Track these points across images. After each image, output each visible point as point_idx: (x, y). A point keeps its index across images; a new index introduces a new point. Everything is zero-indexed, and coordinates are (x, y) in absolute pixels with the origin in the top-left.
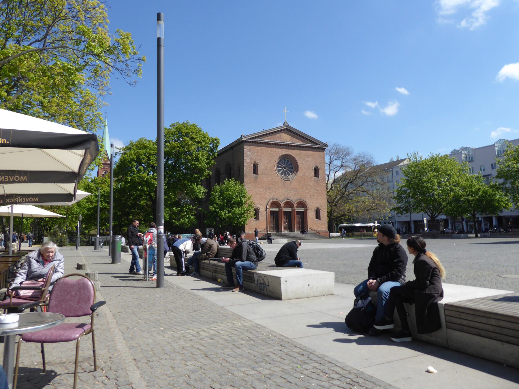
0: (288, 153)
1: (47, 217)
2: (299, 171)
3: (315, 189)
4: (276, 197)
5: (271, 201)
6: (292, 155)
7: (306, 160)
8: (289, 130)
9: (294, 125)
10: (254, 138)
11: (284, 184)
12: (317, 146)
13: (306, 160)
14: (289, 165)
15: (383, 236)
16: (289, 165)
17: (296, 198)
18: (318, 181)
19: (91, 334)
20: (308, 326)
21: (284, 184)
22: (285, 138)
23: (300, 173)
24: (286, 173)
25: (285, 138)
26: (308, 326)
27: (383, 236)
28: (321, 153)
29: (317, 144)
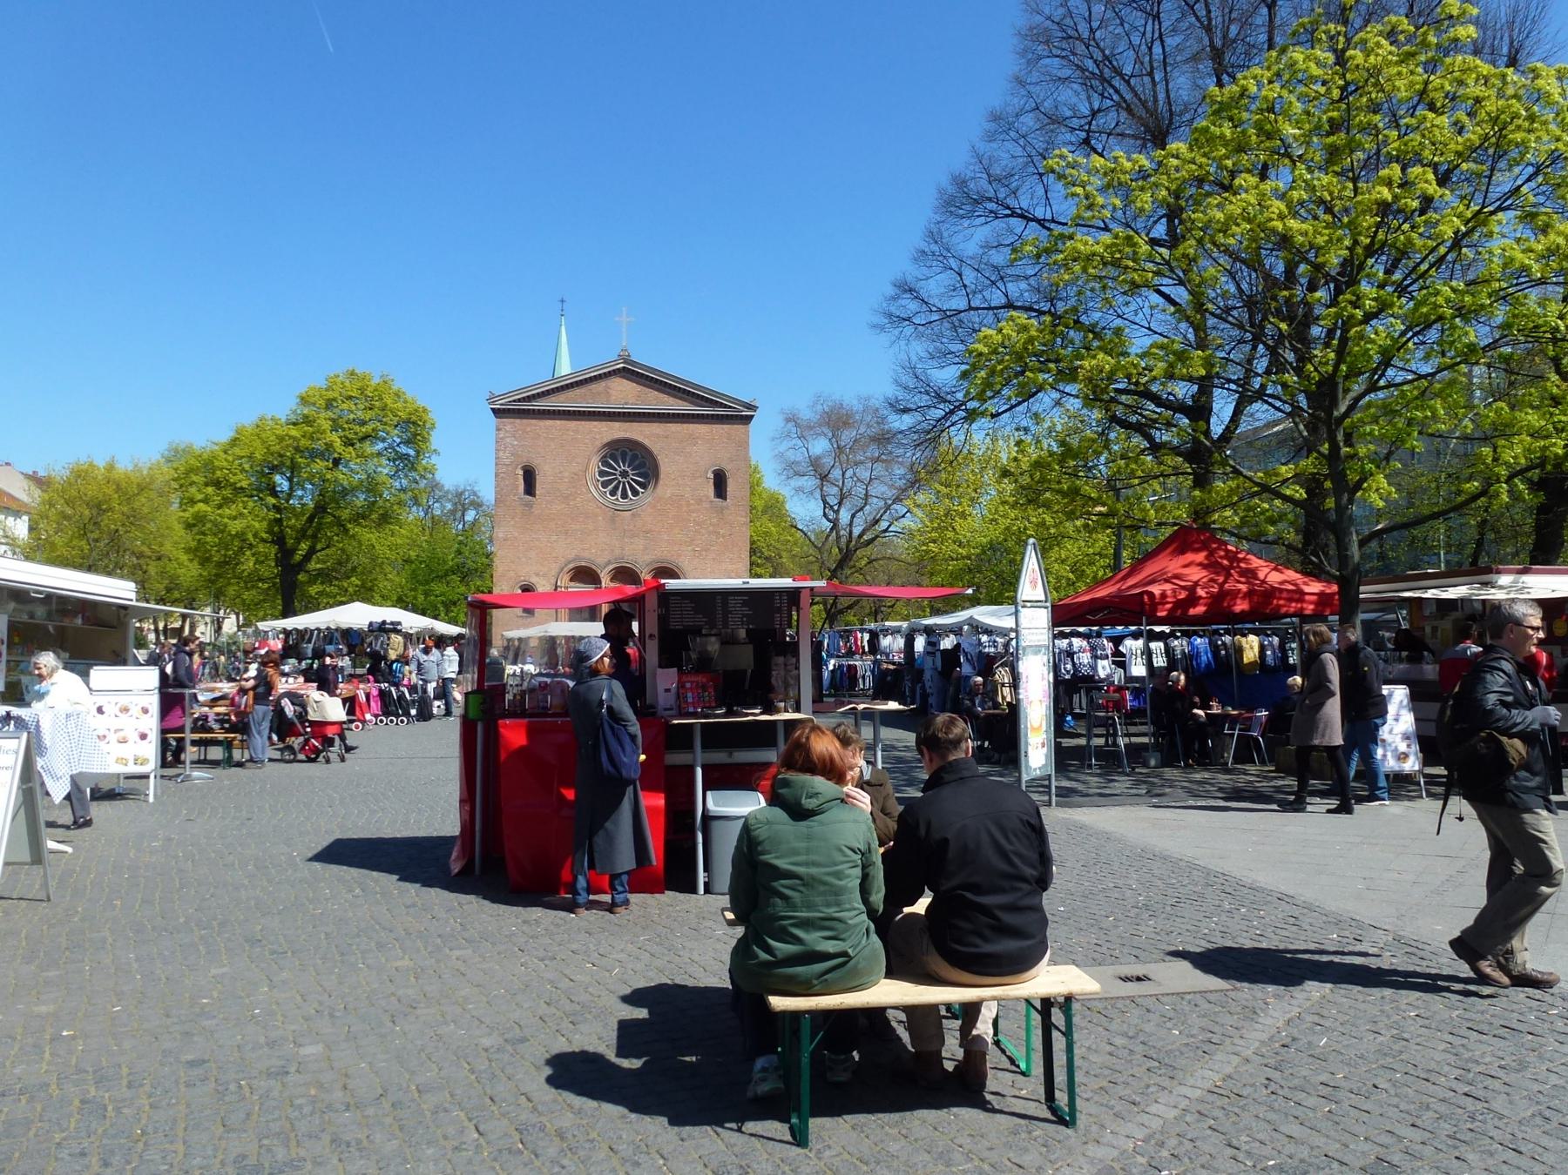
0: (628, 435)
2: (661, 482)
3: (710, 533)
4: (586, 554)
5: (571, 566)
6: (640, 439)
7: (684, 453)
8: (630, 372)
9: (649, 357)
10: (524, 399)
11: (613, 520)
12: (721, 412)
13: (684, 453)
14: (632, 466)
15: (800, 1138)
16: (632, 466)
17: (648, 558)
18: (722, 509)
19: (1472, 975)
20: (342, 853)
21: (613, 520)
22: (624, 394)
23: (666, 487)
24: (611, 484)
25: (624, 394)
26: (342, 853)
27: (800, 1138)
28: (737, 429)
29: (722, 405)
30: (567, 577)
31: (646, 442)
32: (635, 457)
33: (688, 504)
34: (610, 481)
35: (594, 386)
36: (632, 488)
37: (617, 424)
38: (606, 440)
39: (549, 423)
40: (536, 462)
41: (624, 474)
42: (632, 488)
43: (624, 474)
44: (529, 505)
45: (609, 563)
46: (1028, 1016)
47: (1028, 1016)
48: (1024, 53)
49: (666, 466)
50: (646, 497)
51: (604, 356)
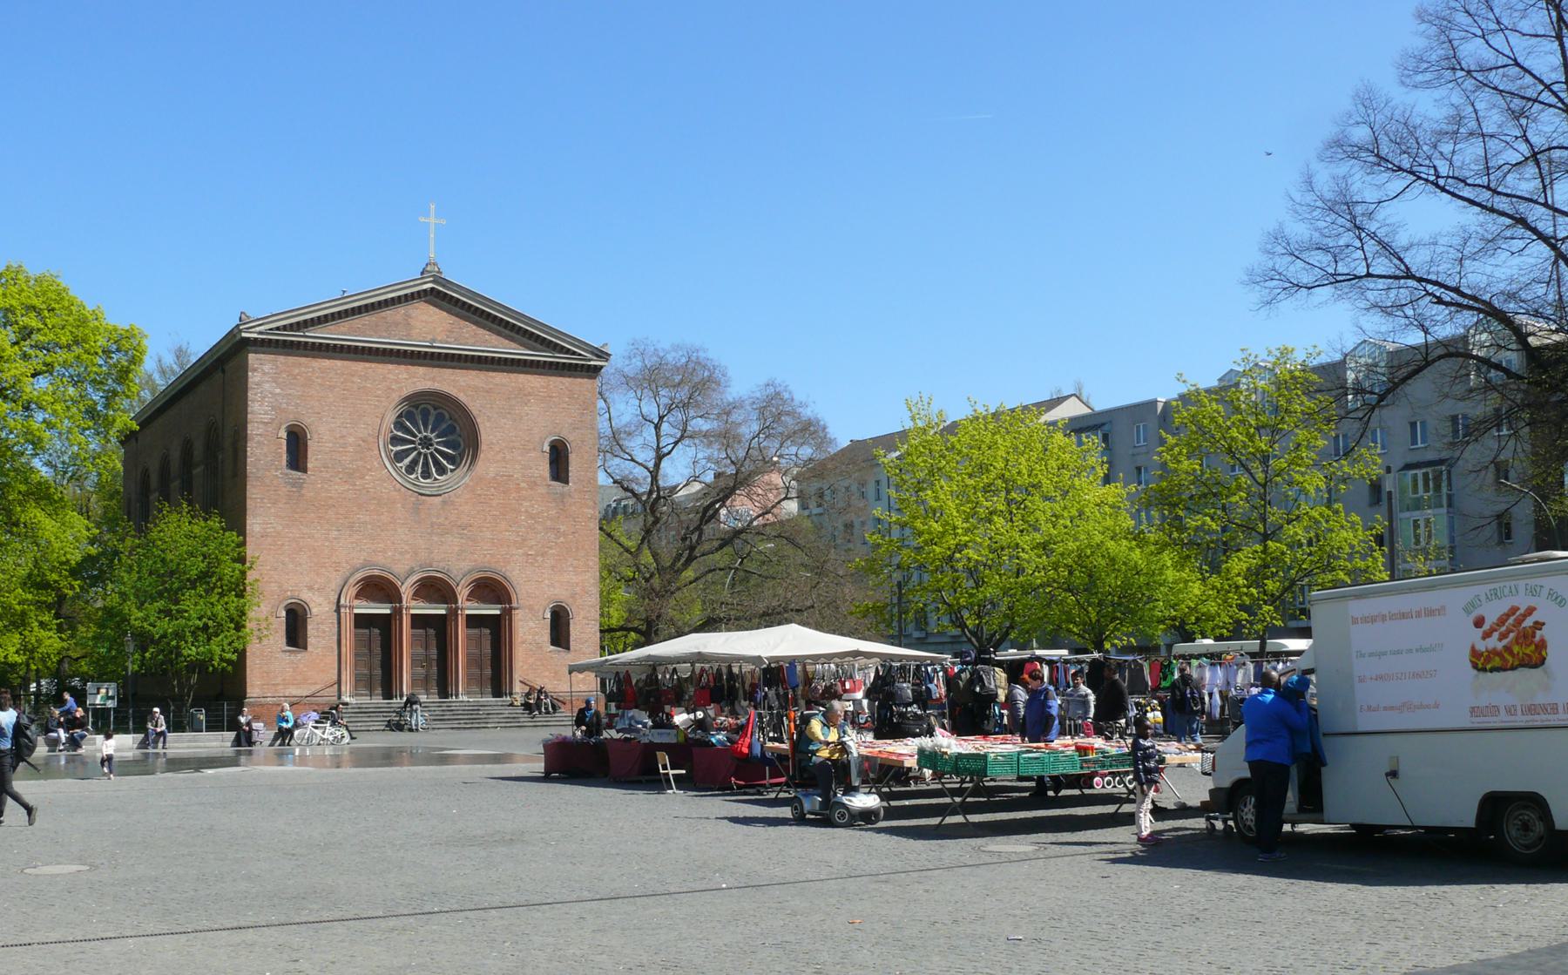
0: (437, 386)
4: (380, 559)
5: (359, 576)
7: (514, 416)
8: (441, 296)
10: (291, 327)
12: (563, 359)
14: (438, 433)
16: (438, 433)
17: (465, 565)
22: (430, 327)
23: (488, 464)
25: (430, 327)
29: (568, 351)
30: (353, 591)
31: (462, 398)
32: (440, 418)
33: (519, 489)
34: (406, 453)
35: (389, 314)
36: (437, 463)
37: (421, 370)
38: (406, 392)
39: (326, 363)
40: (308, 420)
41: (426, 442)
42: (437, 463)
43: (426, 442)
44: (298, 485)
45: (411, 572)
46: (176, 764)
47: (176, 764)
48: (116, 330)
49: (488, 433)
50: (456, 480)
51: (403, 272)
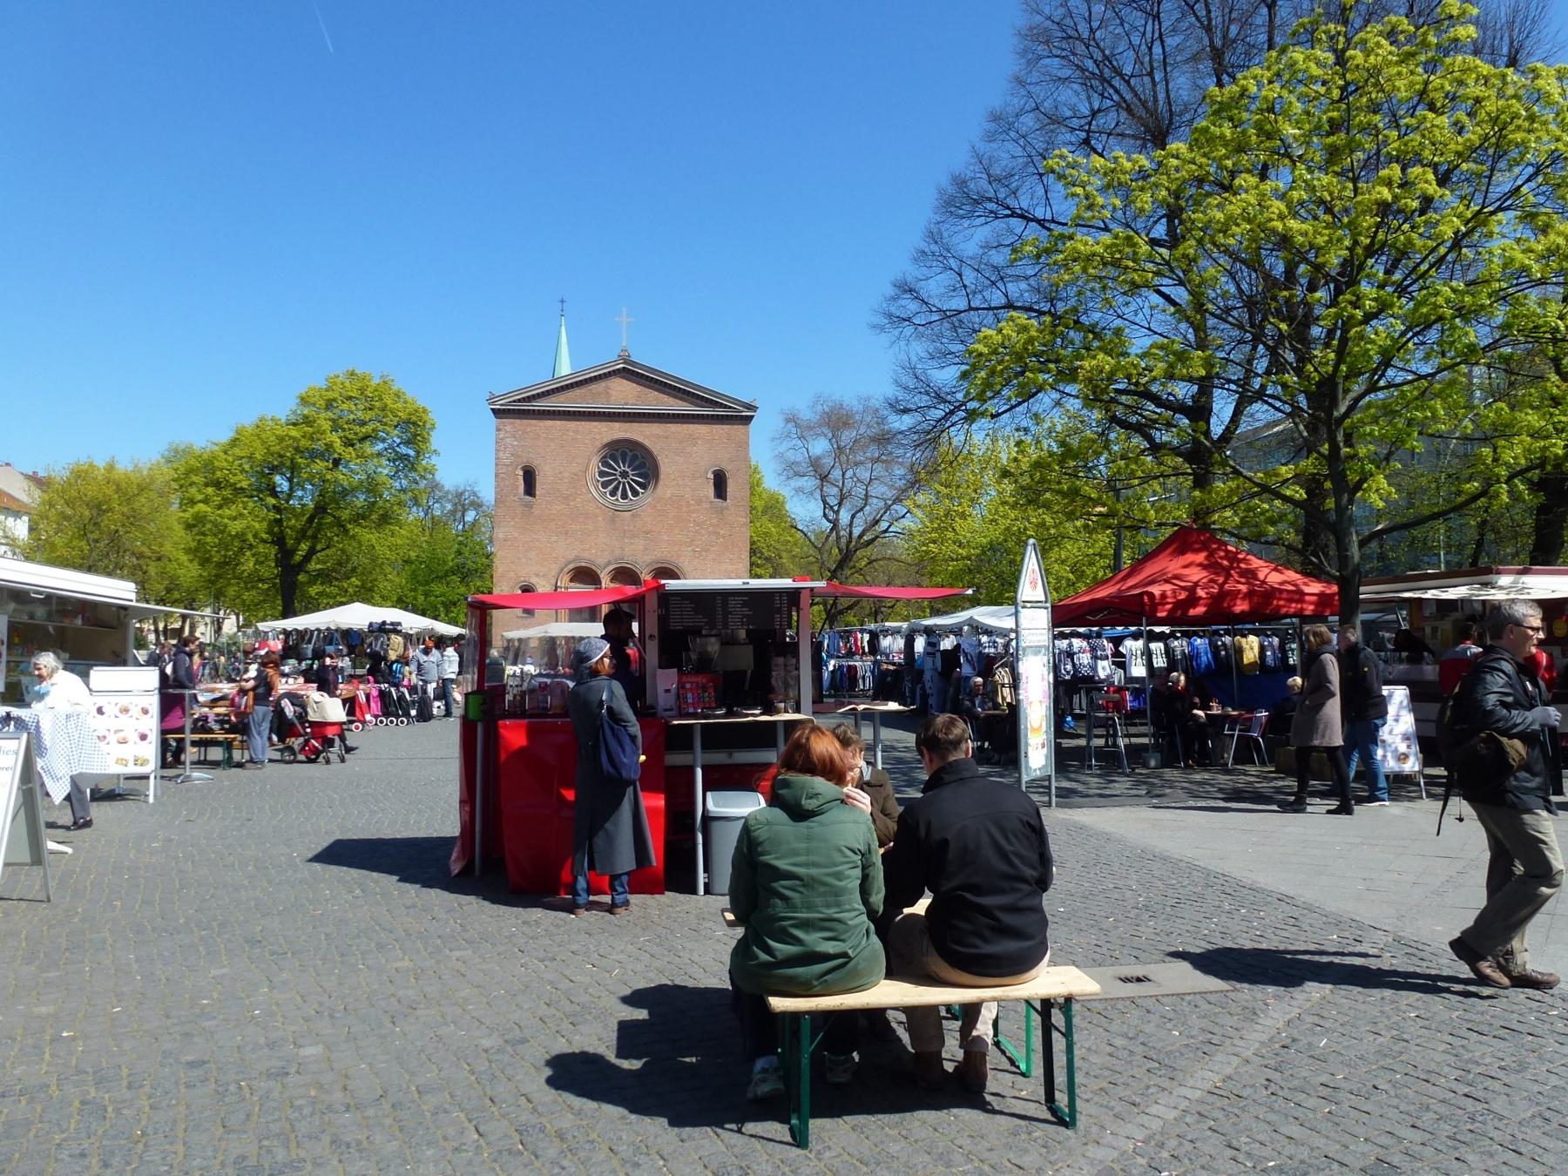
0: (628, 436)
1: (896, 1009)
2: (661, 482)
3: (710, 533)
4: (586, 555)
5: (571, 566)
6: (640, 439)
7: (684, 454)
8: (630, 372)
9: (649, 358)
10: (524, 400)
11: (613, 521)
12: (721, 412)
13: (684, 454)
14: (632, 466)
15: (800, 1139)
16: (632, 466)
17: (648, 559)
18: (722, 509)
20: (342, 853)
21: (613, 521)
22: (624, 394)
23: (666, 487)
24: (611, 484)
25: (624, 394)
26: (342, 853)
27: (800, 1139)
28: (737, 429)
29: (722, 405)
30: (567, 578)
31: (646, 443)
32: (635, 457)
33: (688, 505)
34: (610, 482)
35: (594, 387)
36: (632, 488)
37: (617, 425)
38: (606, 441)
39: (549, 423)
40: (536, 463)
41: (624, 474)
42: (632, 488)
43: (624, 474)
44: (529, 506)
45: (609, 563)
46: (1028, 1017)
47: (1028, 1017)
48: (1024, 53)
49: (666, 466)
50: (646, 497)
51: (604, 356)
